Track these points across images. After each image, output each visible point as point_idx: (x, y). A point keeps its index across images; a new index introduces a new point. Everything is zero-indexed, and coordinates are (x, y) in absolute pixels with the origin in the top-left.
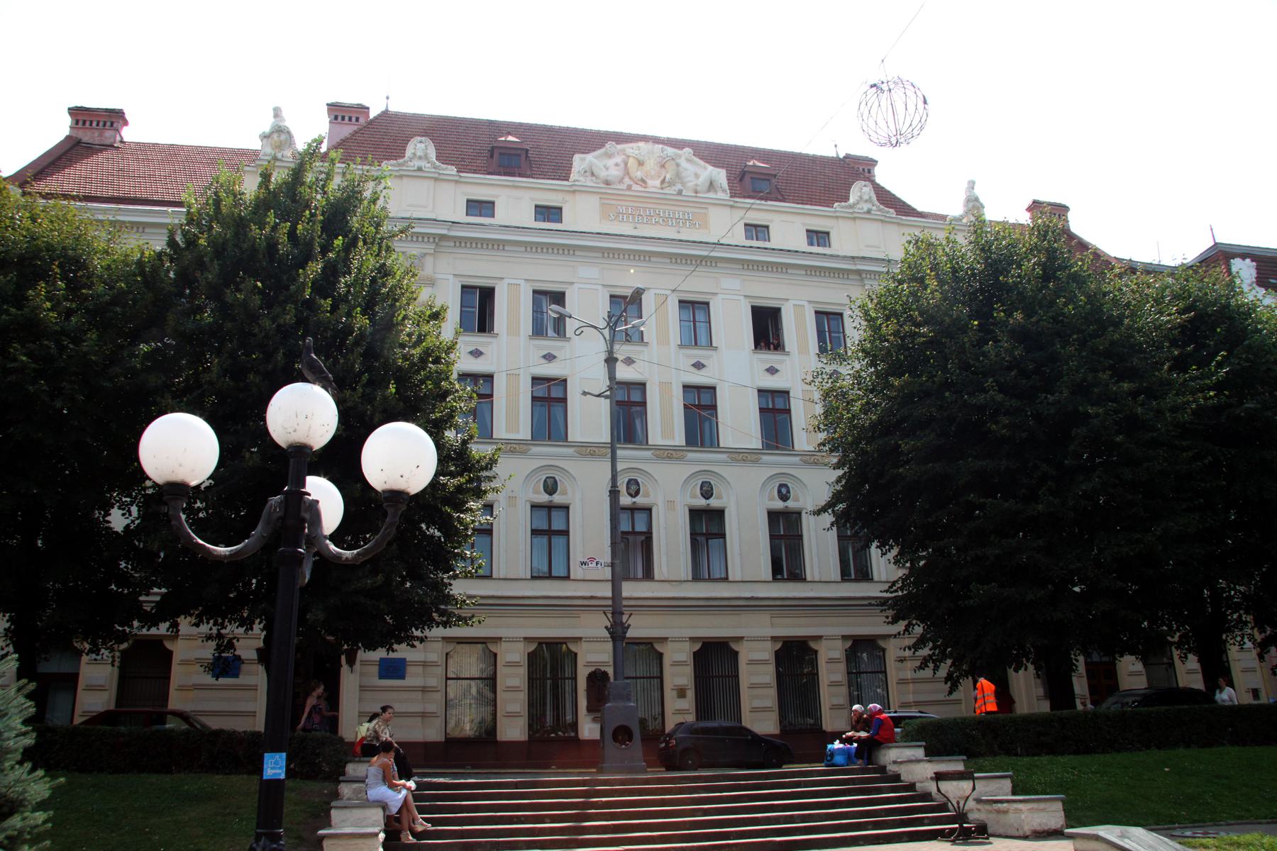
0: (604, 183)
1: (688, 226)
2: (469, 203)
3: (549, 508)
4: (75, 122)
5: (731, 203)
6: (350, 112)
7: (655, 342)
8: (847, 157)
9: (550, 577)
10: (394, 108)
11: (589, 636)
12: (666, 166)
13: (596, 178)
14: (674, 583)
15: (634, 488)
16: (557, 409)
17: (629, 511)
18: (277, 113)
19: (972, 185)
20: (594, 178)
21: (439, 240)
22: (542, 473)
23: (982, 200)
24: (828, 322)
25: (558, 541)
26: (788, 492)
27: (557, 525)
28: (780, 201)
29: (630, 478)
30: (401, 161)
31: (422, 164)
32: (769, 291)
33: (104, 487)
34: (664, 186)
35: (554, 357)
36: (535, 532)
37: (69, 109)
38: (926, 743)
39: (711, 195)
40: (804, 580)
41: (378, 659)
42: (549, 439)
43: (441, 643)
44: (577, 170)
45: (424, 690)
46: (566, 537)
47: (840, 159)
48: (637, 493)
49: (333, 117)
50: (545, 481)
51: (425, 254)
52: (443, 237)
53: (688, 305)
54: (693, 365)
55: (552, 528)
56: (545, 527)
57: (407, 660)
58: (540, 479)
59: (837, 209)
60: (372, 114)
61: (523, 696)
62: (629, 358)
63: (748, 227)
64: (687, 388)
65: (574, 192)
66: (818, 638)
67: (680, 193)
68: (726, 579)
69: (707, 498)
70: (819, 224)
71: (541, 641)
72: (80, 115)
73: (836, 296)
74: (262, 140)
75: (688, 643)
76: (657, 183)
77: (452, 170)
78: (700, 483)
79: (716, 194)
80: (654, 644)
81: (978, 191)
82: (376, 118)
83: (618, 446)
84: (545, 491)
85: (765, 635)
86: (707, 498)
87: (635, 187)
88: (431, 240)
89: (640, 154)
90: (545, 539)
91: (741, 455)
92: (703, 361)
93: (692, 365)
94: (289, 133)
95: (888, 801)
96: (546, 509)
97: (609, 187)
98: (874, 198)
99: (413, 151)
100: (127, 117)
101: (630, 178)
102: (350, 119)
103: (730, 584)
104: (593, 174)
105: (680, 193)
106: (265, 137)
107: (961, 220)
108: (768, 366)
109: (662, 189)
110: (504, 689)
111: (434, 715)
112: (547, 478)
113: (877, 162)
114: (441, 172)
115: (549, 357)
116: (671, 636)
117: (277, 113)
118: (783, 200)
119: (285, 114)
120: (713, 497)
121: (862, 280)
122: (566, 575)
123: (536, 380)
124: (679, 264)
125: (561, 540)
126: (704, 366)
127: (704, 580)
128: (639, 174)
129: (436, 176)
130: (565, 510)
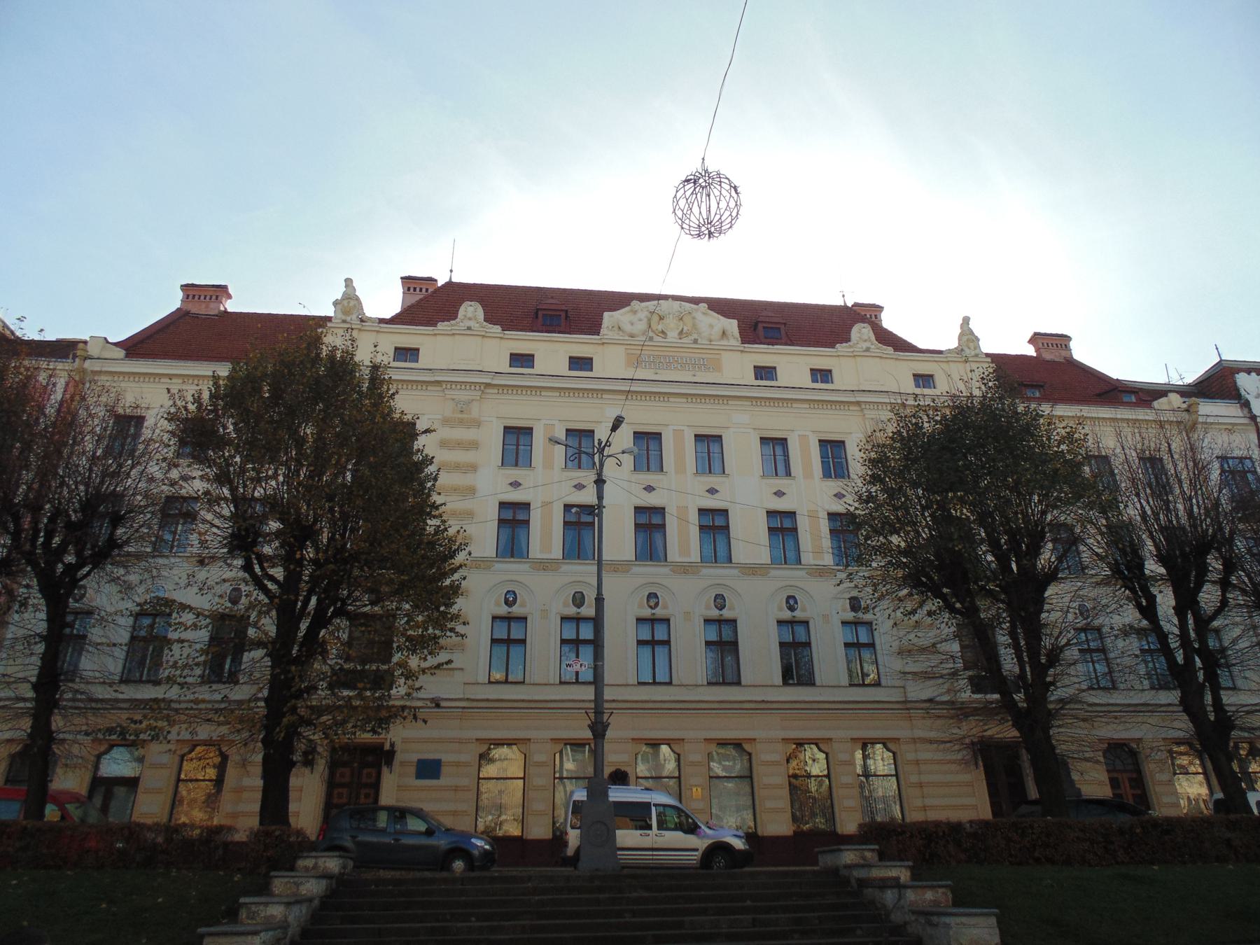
3: (792, 623)
5: (742, 349)
6: (421, 284)
8: (856, 305)
10: (455, 280)
12: (684, 319)
14: (691, 688)
16: (657, 537)
17: (717, 623)
18: (348, 282)
19: (966, 320)
20: (621, 333)
24: (833, 451)
25: (515, 650)
26: (796, 602)
27: (660, 634)
28: (790, 345)
31: (472, 324)
32: (776, 422)
35: (520, 484)
36: (640, 643)
37: (182, 286)
39: (724, 342)
40: (813, 684)
42: (786, 563)
45: (456, 789)
46: (668, 647)
48: (657, 604)
49: (406, 289)
50: (574, 595)
51: (473, 400)
52: (488, 385)
54: (775, 493)
55: (580, 638)
56: (649, 638)
60: (440, 284)
65: (603, 344)
66: (752, 740)
67: (695, 341)
68: (738, 683)
70: (822, 363)
77: (497, 329)
80: (744, 745)
82: (443, 286)
84: (716, 607)
86: (721, 610)
87: (656, 338)
88: (478, 388)
90: (647, 651)
94: (358, 299)
98: (873, 338)
99: (464, 313)
100: (231, 291)
101: (653, 331)
102: (421, 290)
103: (743, 688)
105: (695, 341)
106: (336, 303)
108: (835, 492)
112: (576, 592)
113: (883, 308)
115: (516, 484)
117: (348, 282)
118: (792, 345)
121: (862, 410)
122: (667, 680)
123: (702, 512)
126: (717, 491)
128: (660, 328)
129: (483, 334)
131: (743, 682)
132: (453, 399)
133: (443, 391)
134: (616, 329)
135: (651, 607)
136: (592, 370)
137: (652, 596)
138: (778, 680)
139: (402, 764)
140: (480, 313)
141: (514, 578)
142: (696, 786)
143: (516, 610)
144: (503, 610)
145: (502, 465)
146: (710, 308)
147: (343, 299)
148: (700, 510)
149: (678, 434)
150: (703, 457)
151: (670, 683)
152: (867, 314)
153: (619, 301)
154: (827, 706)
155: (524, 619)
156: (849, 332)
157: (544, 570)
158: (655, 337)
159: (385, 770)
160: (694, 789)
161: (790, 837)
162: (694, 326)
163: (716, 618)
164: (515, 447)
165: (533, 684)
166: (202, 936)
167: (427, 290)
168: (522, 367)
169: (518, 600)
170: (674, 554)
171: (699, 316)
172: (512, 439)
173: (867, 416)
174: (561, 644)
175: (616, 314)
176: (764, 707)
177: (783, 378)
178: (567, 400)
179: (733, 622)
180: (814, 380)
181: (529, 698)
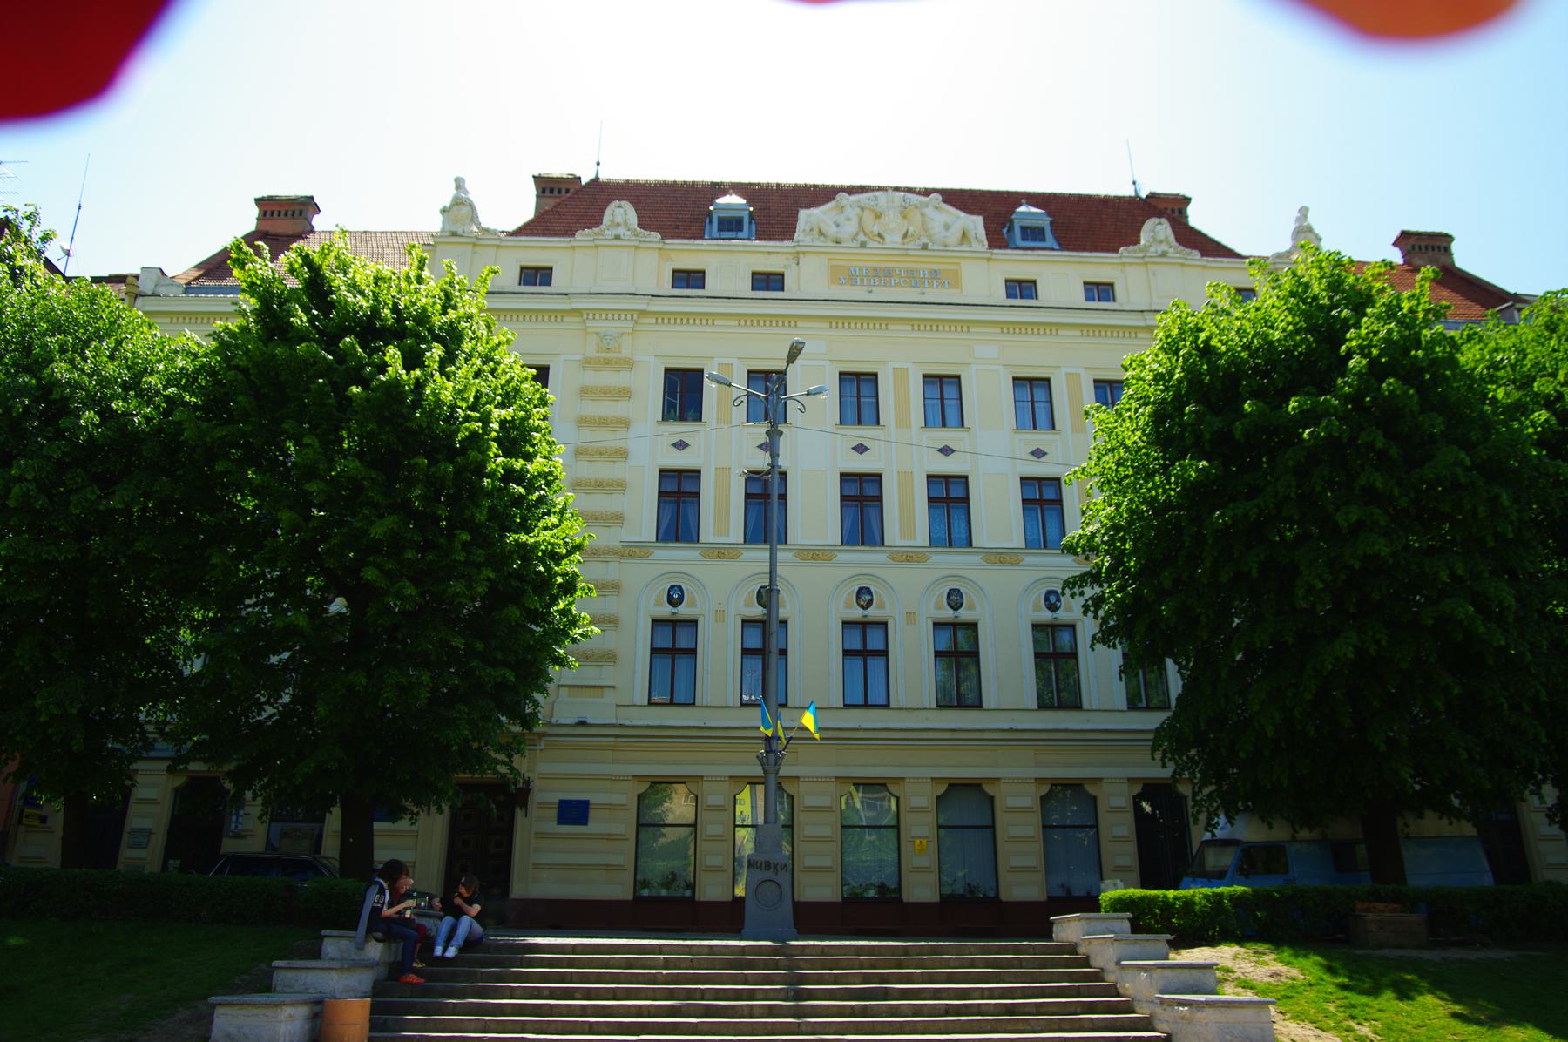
0: (833, 242)
1: (935, 286)
2: (676, 274)
4: (262, 213)
7: (893, 423)
8: (1152, 196)
9: (866, 705)
10: (603, 177)
11: (807, 775)
13: (825, 236)
15: (867, 597)
16: (872, 513)
18: (459, 183)
19: (1304, 212)
21: (638, 317)
22: (853, 583)
23: (1317, 230)
24: (1108, 390)
25: (875, 664)
27: (875, 643)
29: (862, 586)
30: (596, 230)
31: (621, 231)
33: (1161, 611)
34: (906, 241)
36: (847, 653)
38: (1133, 913)
39: (965, 248)
41: (557, 802)
43: (727, 783)
44: (802, 229)
45: (609, 837)
46: (884, 658)
47: (1140, 199)
48: (870, 603)
49: (540, 190)
50: (759, 591)
51: (622, 334)
52: (643, 313)
53: (1024, 382)
57: (591, 802)
58: (943, 592)
59: (1124, 254)
61: (1132, 848)
62: (861, 445)
63: (1011, 284)
64: (931, 478)
66: (1097, 781)
69: (956, 609)
70: (1022, 271)
71: (1054, 782)
72: (269, 206)
73: (1114, 358)
74: (443, 215)
75: (1126, 785)
76: (898, 238)
78: (947, 591)
79: (971, 246)
80: (783, 784)
81: (1312, 220)
82: (588, 184)
83: (779, 547)
85: (918, 776)
86: (956, 609)
88: (629, 317)
89: (877, 205)
90: (857, 663)
91: (998, 557)
92: (1044, 449)
93: (853, 448)
94: (471, 205)
95: (983, 994)
96: (861, 626)
97: (838, 245)
98: (1172, 238)
99: (611, 218)
101: (865, 234)
104: (821, 233)
107: (1288, 257)
109: (904, 244)
110: (1006, 839)
111: (720, 869)
112: (761, 587)
114: (642, 240)
116: (803, 775)
117: (459, 183)
119: (468, 186)
120: (963, 608)
122: (884, 703)
124: (598, 320)
125: (879, 662)
127: (1141, 709)
128: (876, 229)
130: (1071, 629)
131: (985, 705)
132: (597, 334)
133: (584, 322)
134: (816, 232)
135: (862, 607)
136: (783, 290)
137: (862, 591)
138: (1123, 704)
139: (542, 805)
140: (633, 218)
141: (679, 568)
142: (919, 837)
143: (683, 611)
144: (666, 611)
145: (841, 423)
146: (945, 201)
147: (452, 206)
148: (1022, 479)
149: (900, 374)
150: (933, 405)
151: (887, 706)
152: (1172, 208)
153: (819, 195)
154: (1044, 736)
155: (693, 623)
156: (602, 212)
157: (908, 561)
158: (871, 244)
159: (519, 813)
160: (917, 842)
161: (936, 903)
162: (924, 226)
163: (951, 621)
164: (856, 399)
165: (707, 707)
166: (213, 1006)
167: (567, 191)
168: (688, 287)
169: (874, 601)
170: (893, 535)
171: (929, 211)
172: (851, 389)
173: (589, 330)
174: (742, 654)
175: (815, 211)
176: (1014, 738)
177: (1047, 294)
178: (1119, 341)
179: (973, 627)
180: (1089, 298)
181: (657, 723)
